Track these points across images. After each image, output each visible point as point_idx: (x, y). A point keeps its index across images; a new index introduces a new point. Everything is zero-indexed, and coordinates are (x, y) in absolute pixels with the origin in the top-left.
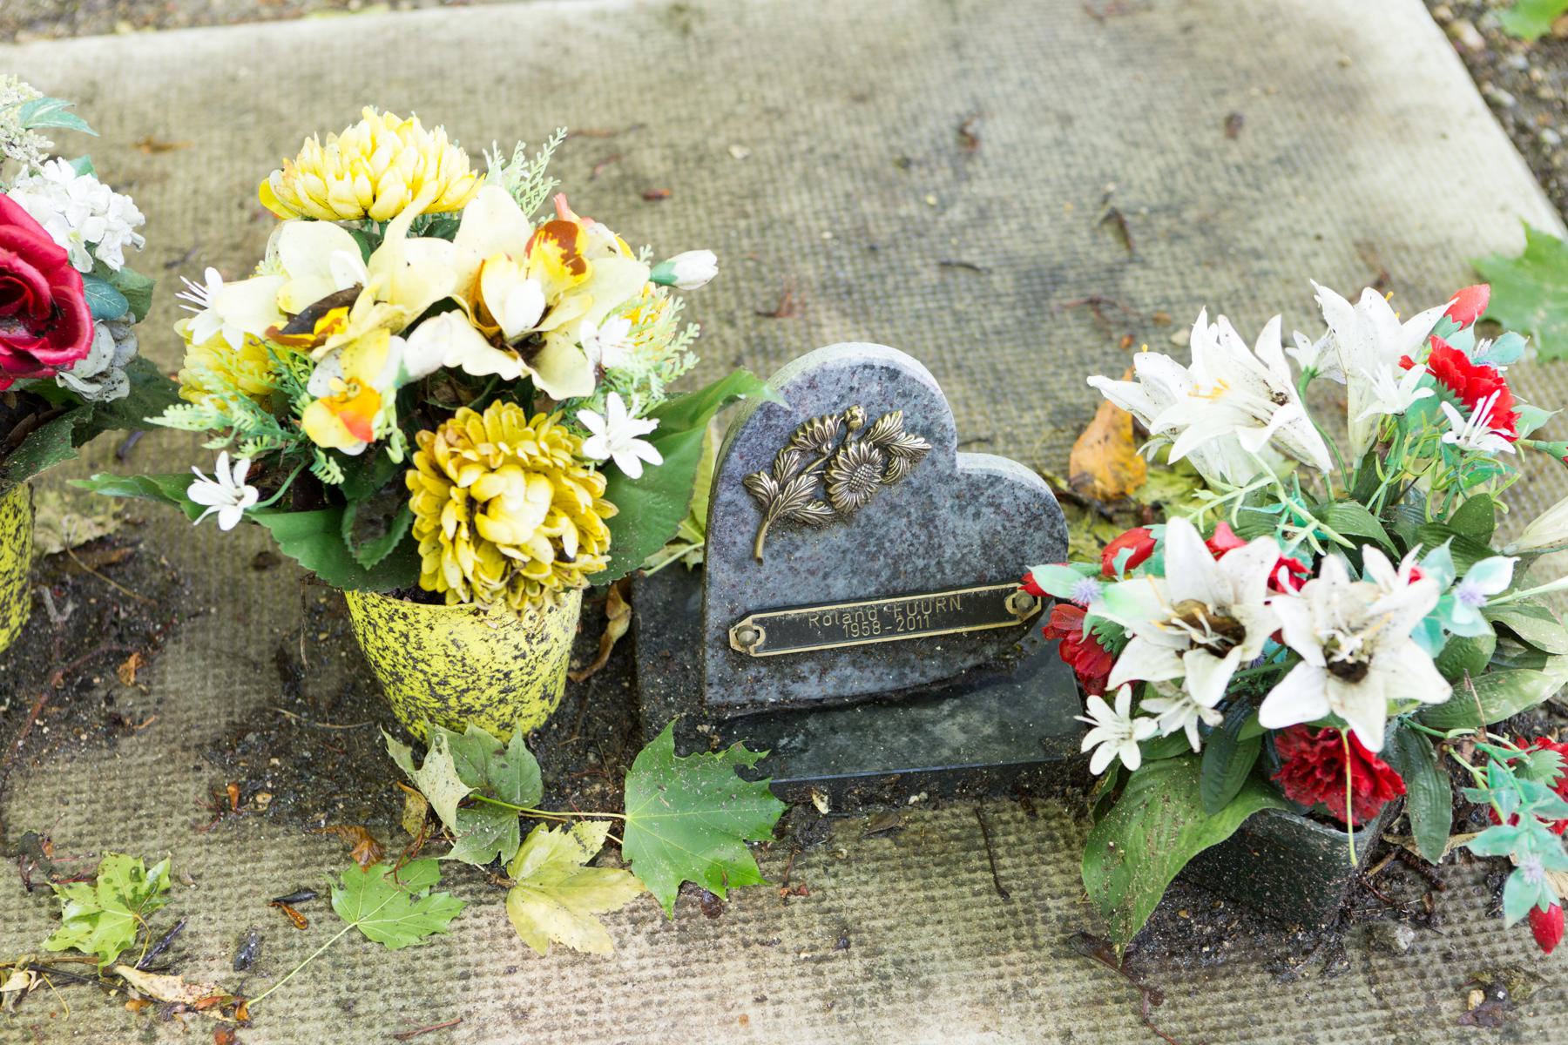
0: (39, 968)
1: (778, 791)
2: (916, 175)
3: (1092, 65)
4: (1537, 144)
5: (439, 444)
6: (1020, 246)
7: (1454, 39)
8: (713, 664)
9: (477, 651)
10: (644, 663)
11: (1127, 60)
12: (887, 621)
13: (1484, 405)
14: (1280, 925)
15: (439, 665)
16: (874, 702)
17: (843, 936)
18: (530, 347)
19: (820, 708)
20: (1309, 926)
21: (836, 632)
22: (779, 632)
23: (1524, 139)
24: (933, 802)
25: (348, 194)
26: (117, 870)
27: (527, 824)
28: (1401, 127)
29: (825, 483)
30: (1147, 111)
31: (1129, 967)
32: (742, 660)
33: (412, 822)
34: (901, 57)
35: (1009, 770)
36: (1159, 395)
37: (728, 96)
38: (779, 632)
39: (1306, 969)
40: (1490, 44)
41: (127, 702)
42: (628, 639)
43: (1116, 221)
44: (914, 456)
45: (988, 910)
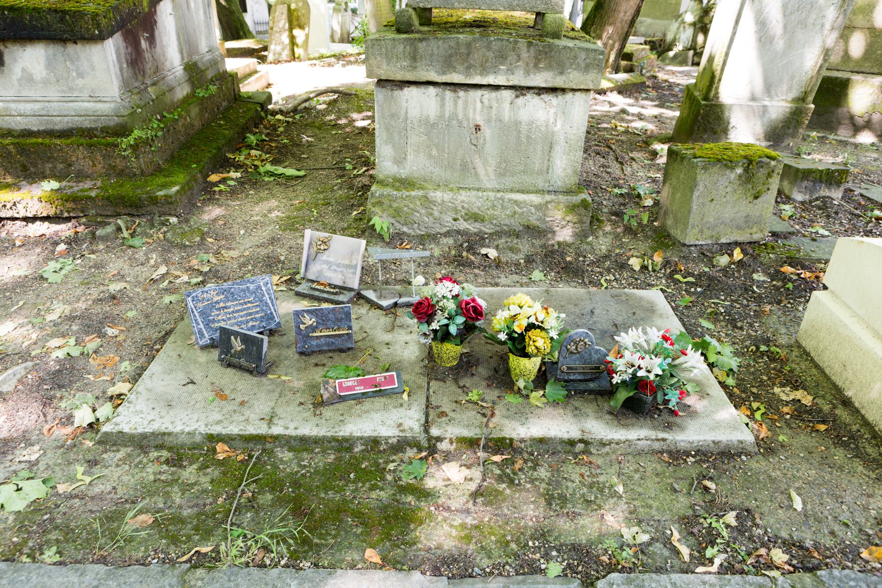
0: (466, 401)
1: (567, 390)
2: (584, 316)
3: (612, 304)
4: (683, 321)
5: (530, 333)
6: (600, 327)
7: (670, 305)
8: (559, 372)
9: (528, 365)
10: (548, 373)
11: (617, 303)
12: (583, 368)
13: (669, 342)
14: (638, 413)
15: (522, 367)
16: (580, 381)
17: (576, 409)
18: (542, 322)
19: (573, 380)
20: (642, 414)
21: (576, 369)
22: (569, 368)
23: (681, 320)
24: (589, 394)
25: (518, 302)
26: (475, 391)
27: (532, 391)
28: (661, 316)
29: (577, 348)
30: (620, 310)
31: (616, 416)
32: (563, 372)
33: (516, 388)
34: (582, 300)
35: (600, 391)
36: (624, 339)
37: (555, 303)
38: (569, 368)
39: (642, 419)
40: (676, 306)
41: (474, 372)
42: (545, 370)
43: (616, 325)
44: (589, 345)
45: (597, 408)
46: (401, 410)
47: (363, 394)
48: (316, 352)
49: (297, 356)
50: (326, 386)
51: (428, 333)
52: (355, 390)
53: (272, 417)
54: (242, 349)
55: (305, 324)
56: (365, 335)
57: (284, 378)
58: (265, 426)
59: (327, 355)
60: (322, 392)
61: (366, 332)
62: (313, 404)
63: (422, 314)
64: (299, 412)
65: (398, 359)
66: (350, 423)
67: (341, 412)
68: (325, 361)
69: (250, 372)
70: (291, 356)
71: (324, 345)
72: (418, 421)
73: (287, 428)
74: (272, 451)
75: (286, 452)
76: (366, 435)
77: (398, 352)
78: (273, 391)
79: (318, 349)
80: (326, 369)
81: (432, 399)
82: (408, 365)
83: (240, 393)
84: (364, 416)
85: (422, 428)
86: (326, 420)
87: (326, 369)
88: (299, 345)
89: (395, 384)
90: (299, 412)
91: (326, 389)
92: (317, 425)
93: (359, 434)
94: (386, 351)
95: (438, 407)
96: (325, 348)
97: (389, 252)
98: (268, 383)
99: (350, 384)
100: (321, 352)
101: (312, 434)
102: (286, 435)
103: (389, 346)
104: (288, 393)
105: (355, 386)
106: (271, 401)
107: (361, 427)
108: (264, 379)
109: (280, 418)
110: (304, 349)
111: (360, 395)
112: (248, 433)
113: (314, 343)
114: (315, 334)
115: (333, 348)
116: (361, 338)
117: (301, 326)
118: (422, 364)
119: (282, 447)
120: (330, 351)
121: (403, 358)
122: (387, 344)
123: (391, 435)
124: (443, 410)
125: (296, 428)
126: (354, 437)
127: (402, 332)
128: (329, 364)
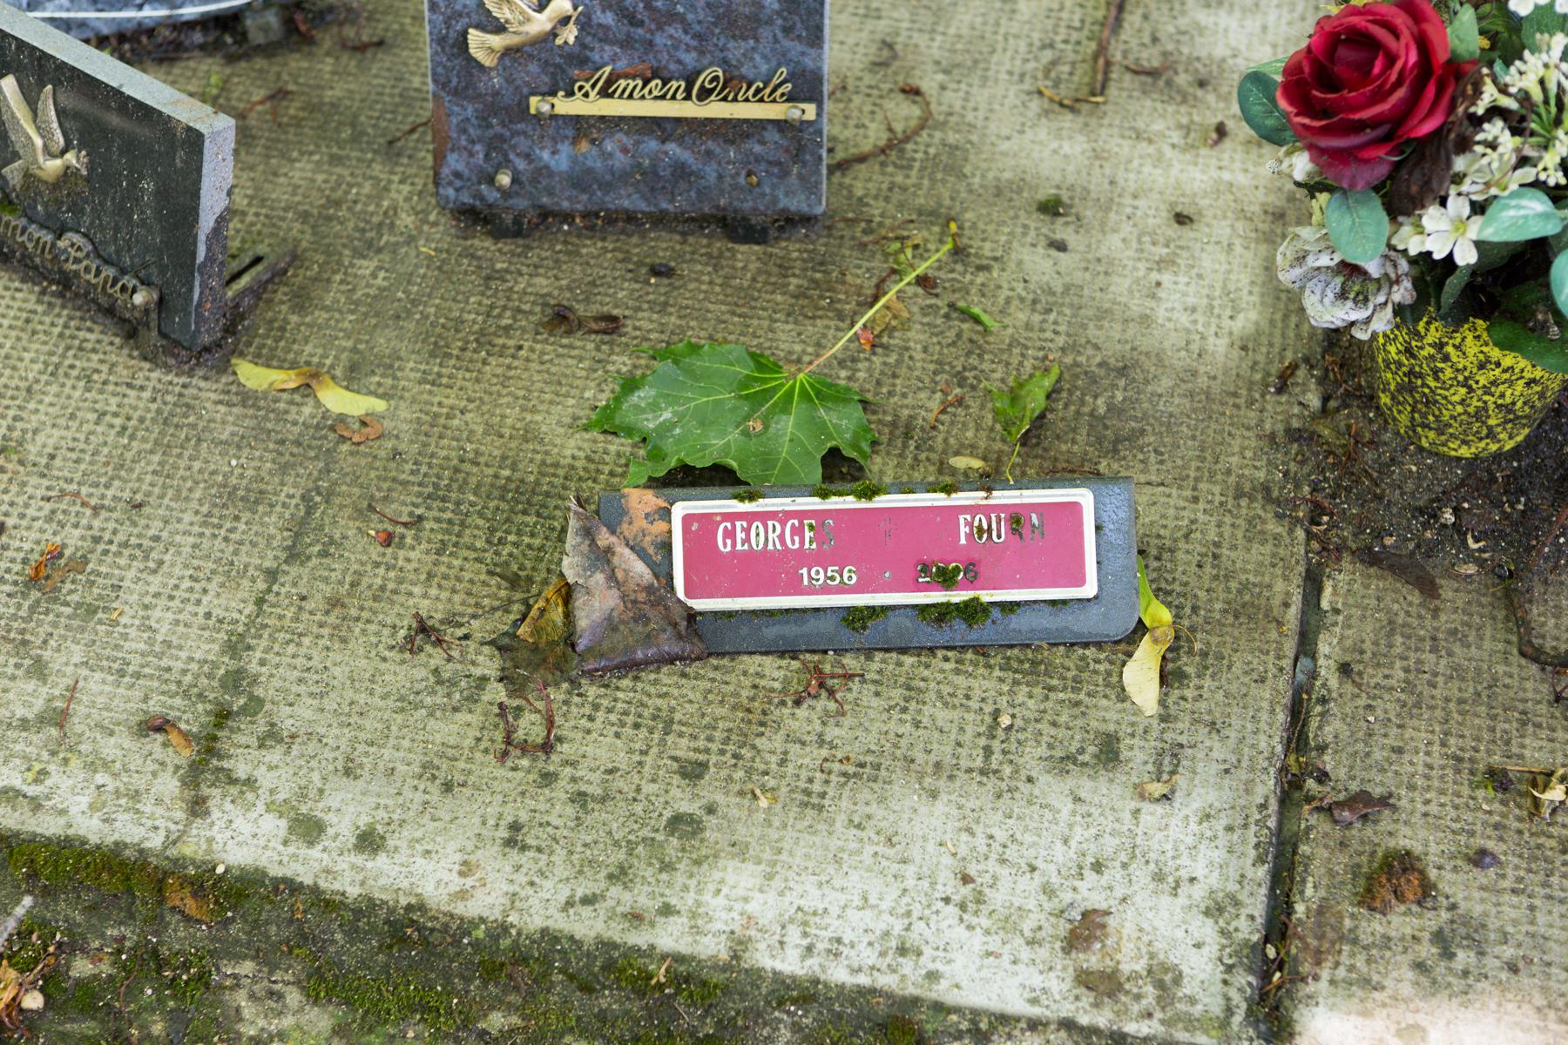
46: (1106, 791)
47: (856, 618)
48: (568, 217)
49: (439, 234)
50: (604, 538)
51: (1373, 268)
52: (796, 588)
53: (223, 716)
54: (68, 173)
55: (500, 28)
56: (904, 113)
57: (337, 400)
58: (169, 785)
59: (637, 247)
60: (571, 567)
61: (912, 92)
62: (504, 646)
63: (1360, 126)
64: (406, 704)
65: (1111, 339)
66: (740, 850)
67: (682, 747)
68: (619, 295)
69: (130, 330)
70: (406, 220)
71: (624, 177)
72: (1215, 910)
73: (308, 829)
74: (202, 978)
75: (294, 997)
76: (839, 975)
77: (1120, 286)
78: (255, 499)
79: (582, 202)
80: (622, 363)
81: (1328, 728)
82: (1179, 403)
83: (37, 486)
84: (843, 805)
85: (1245, 980)
86: (580, 798)
87: (622, 363)
88: (454, 162)
89: (1075, 508)
90: (406, 704)
91: (602, 558)
92: (514, 839)
93: (790, 964)
94: (1039, 265)
95: (1366, 805)
96: (628, 200)
97: (1514, 224)
98: (227, 421)
99: (764, 538)
100: (602, 222)
101: (470, 909)
102: (294, 887)
103: (1062, 231)
104: (346, 527)
105: (803, 558)
106: (231, 575)
107: (813, 900)
108: (205, 390)
109: (271, 737)
110: (492, 195)
111: (827, 625)
112: (48, 826)
113: (560, 158)
114: (566, 106)
115: (679, 203)
116: (875, 135)
117: (474, 36)
118: (1277, 413)
119: (267, 959)
120: (660, 220)
121: (1145, 344)
122: (1051, 208)
123: (1016, 1004)
124: (1406, 839)
125: (369, 842)
126: (756, 974)
127: (1159, 118)
128: (646, 321)
